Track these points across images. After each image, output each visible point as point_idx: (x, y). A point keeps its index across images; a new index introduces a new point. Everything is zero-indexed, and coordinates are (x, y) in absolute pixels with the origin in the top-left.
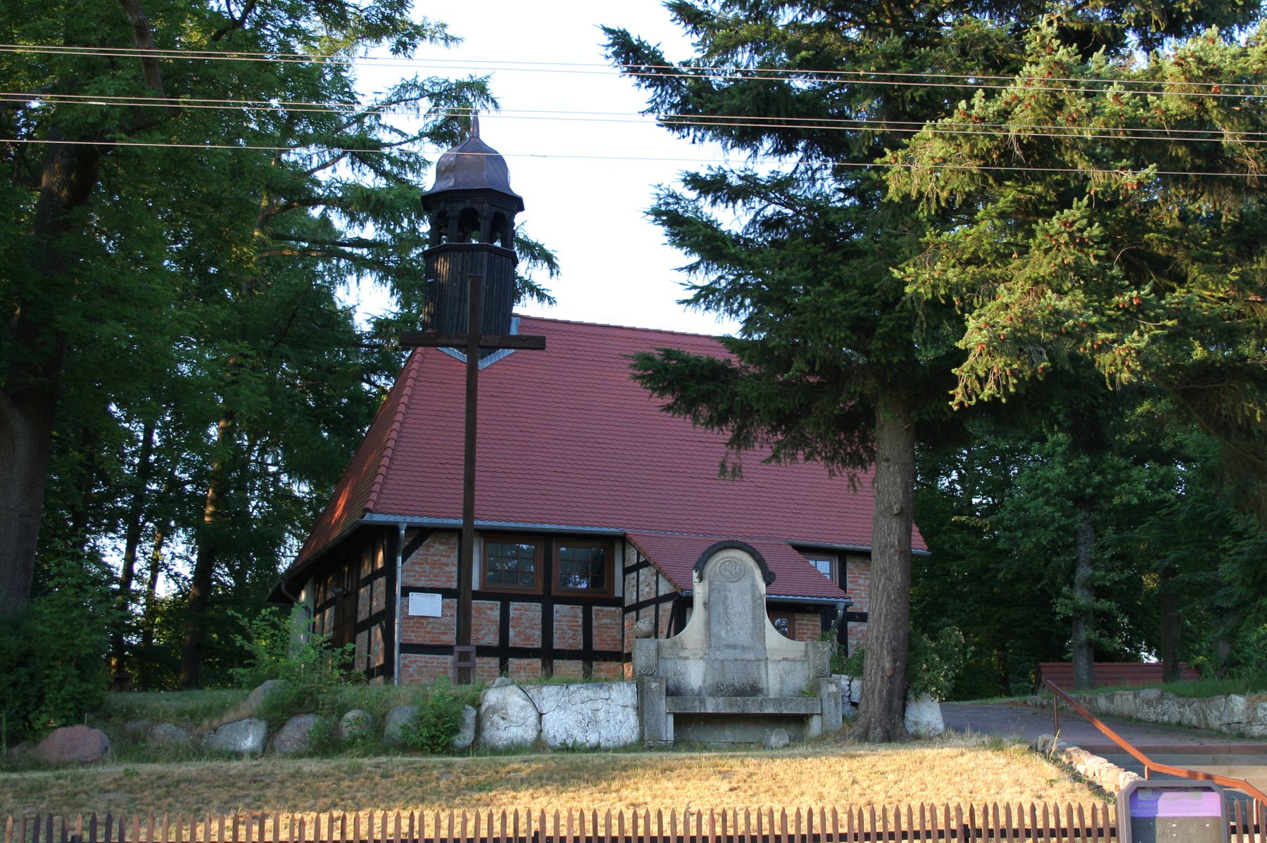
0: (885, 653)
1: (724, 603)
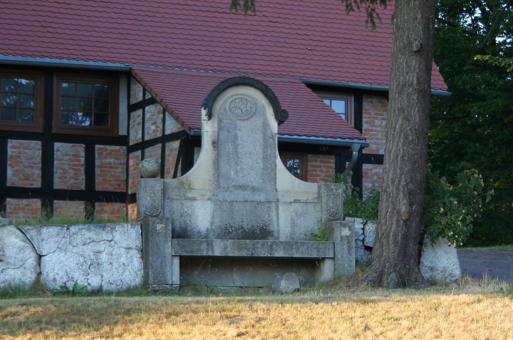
0: (401, 196)
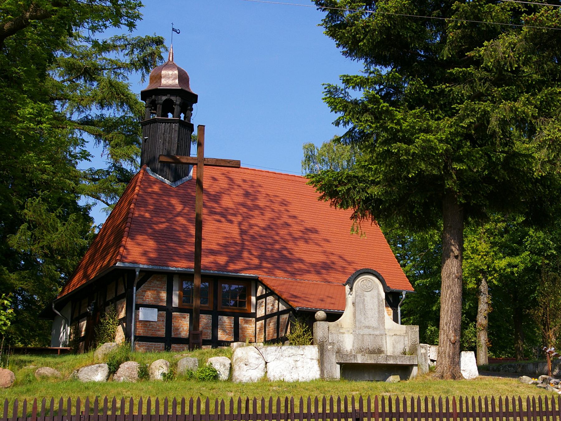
0: (451, 332)
1: (363, 303)
